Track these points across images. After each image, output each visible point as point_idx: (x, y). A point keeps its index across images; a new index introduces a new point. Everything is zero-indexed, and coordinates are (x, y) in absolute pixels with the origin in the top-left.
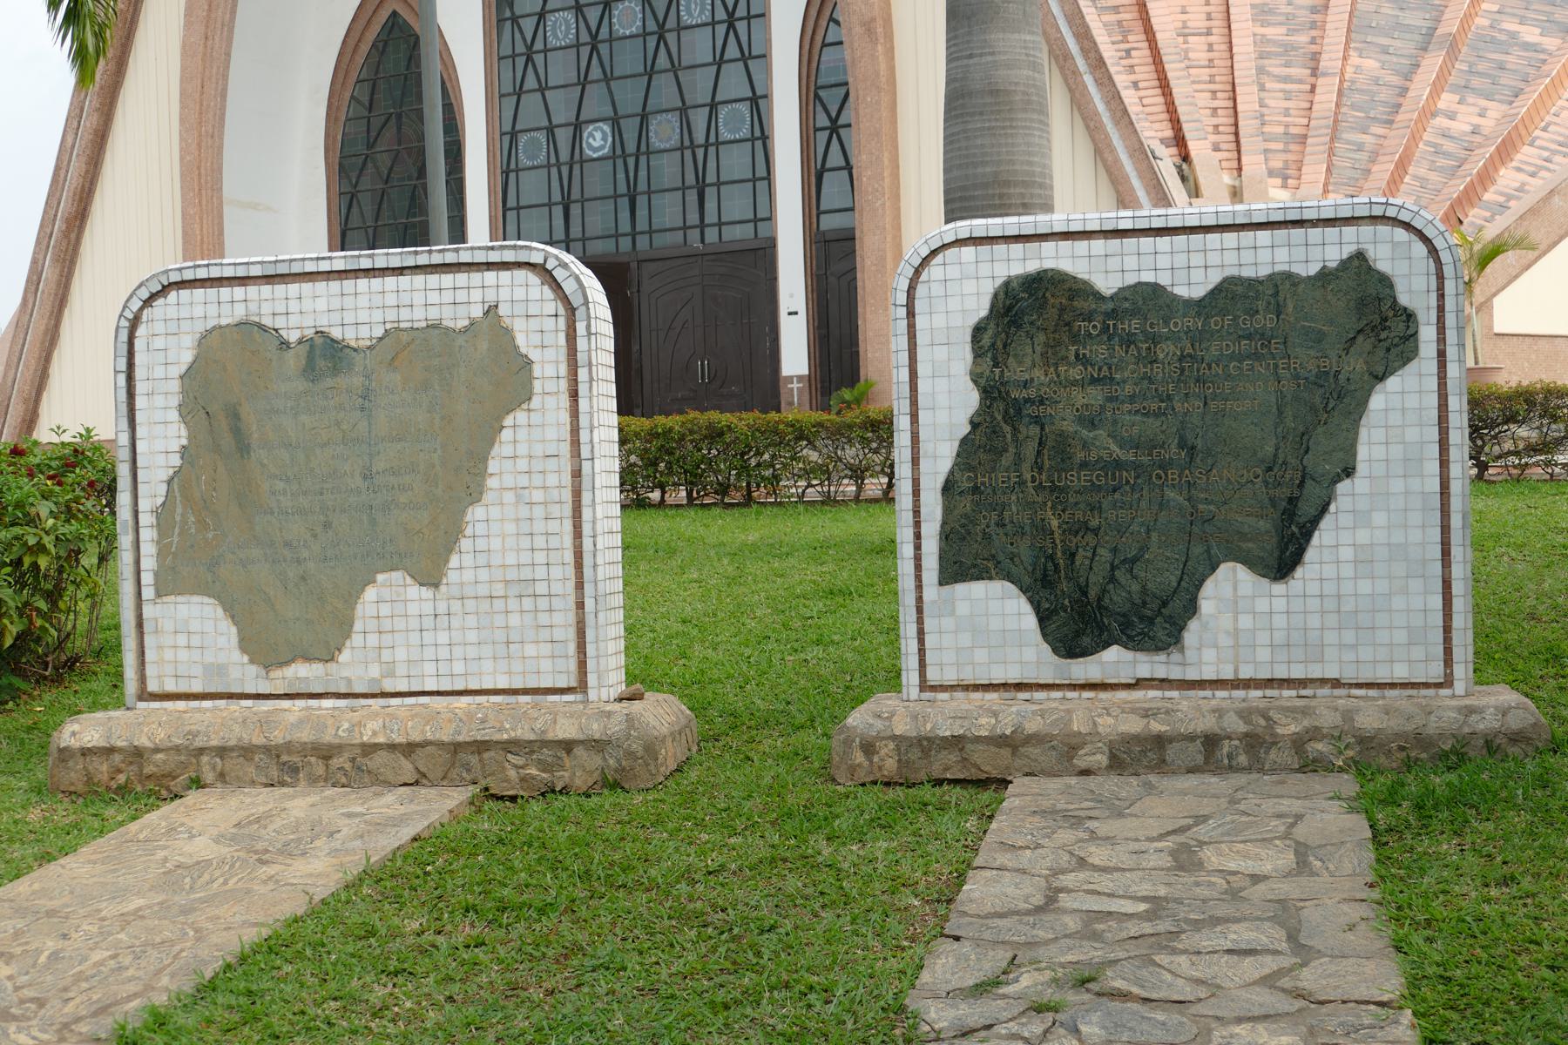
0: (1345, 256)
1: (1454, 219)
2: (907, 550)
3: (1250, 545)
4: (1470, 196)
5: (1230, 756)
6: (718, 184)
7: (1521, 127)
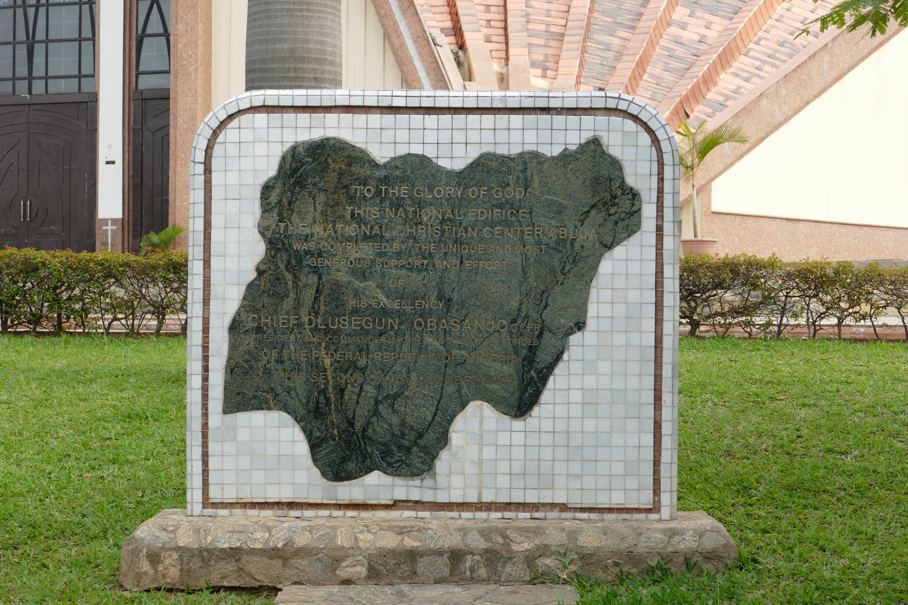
0: (583, 141)
1: (682, 113)
2: (196, 381)
3: (495, 386)
4: (696, 94)
5: (472, 570)
6: (47, 41)
7: (738, 40)
